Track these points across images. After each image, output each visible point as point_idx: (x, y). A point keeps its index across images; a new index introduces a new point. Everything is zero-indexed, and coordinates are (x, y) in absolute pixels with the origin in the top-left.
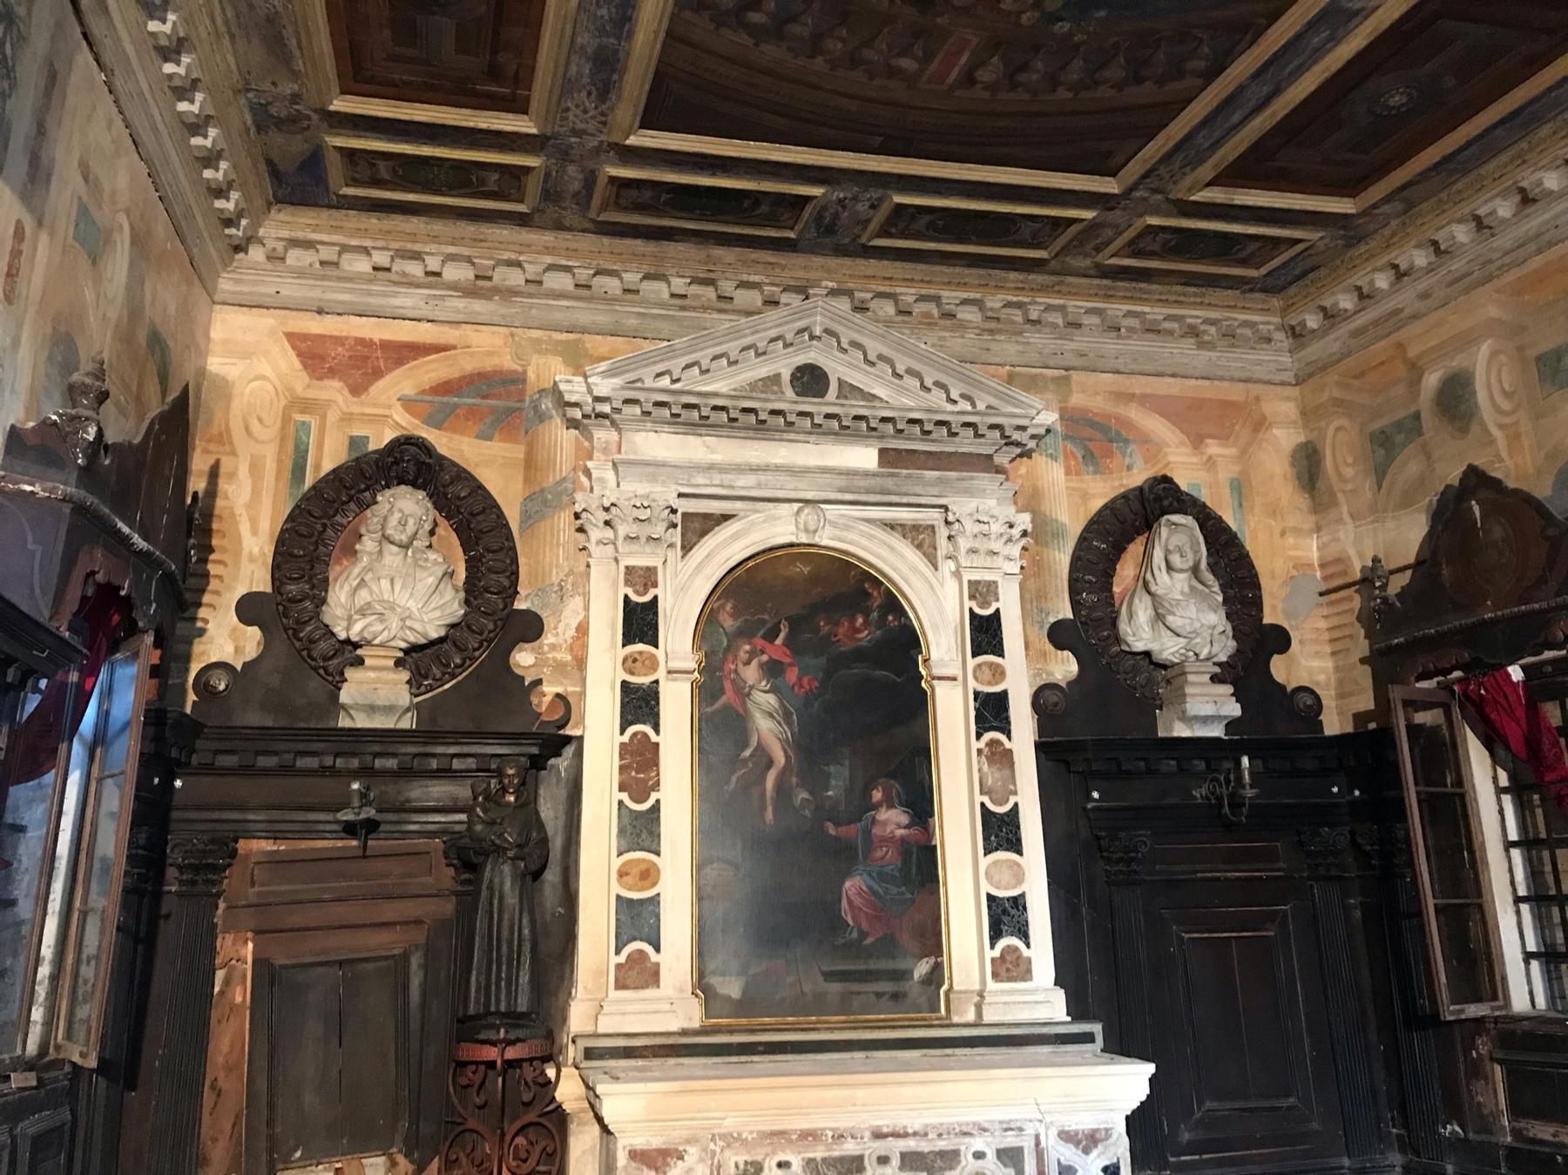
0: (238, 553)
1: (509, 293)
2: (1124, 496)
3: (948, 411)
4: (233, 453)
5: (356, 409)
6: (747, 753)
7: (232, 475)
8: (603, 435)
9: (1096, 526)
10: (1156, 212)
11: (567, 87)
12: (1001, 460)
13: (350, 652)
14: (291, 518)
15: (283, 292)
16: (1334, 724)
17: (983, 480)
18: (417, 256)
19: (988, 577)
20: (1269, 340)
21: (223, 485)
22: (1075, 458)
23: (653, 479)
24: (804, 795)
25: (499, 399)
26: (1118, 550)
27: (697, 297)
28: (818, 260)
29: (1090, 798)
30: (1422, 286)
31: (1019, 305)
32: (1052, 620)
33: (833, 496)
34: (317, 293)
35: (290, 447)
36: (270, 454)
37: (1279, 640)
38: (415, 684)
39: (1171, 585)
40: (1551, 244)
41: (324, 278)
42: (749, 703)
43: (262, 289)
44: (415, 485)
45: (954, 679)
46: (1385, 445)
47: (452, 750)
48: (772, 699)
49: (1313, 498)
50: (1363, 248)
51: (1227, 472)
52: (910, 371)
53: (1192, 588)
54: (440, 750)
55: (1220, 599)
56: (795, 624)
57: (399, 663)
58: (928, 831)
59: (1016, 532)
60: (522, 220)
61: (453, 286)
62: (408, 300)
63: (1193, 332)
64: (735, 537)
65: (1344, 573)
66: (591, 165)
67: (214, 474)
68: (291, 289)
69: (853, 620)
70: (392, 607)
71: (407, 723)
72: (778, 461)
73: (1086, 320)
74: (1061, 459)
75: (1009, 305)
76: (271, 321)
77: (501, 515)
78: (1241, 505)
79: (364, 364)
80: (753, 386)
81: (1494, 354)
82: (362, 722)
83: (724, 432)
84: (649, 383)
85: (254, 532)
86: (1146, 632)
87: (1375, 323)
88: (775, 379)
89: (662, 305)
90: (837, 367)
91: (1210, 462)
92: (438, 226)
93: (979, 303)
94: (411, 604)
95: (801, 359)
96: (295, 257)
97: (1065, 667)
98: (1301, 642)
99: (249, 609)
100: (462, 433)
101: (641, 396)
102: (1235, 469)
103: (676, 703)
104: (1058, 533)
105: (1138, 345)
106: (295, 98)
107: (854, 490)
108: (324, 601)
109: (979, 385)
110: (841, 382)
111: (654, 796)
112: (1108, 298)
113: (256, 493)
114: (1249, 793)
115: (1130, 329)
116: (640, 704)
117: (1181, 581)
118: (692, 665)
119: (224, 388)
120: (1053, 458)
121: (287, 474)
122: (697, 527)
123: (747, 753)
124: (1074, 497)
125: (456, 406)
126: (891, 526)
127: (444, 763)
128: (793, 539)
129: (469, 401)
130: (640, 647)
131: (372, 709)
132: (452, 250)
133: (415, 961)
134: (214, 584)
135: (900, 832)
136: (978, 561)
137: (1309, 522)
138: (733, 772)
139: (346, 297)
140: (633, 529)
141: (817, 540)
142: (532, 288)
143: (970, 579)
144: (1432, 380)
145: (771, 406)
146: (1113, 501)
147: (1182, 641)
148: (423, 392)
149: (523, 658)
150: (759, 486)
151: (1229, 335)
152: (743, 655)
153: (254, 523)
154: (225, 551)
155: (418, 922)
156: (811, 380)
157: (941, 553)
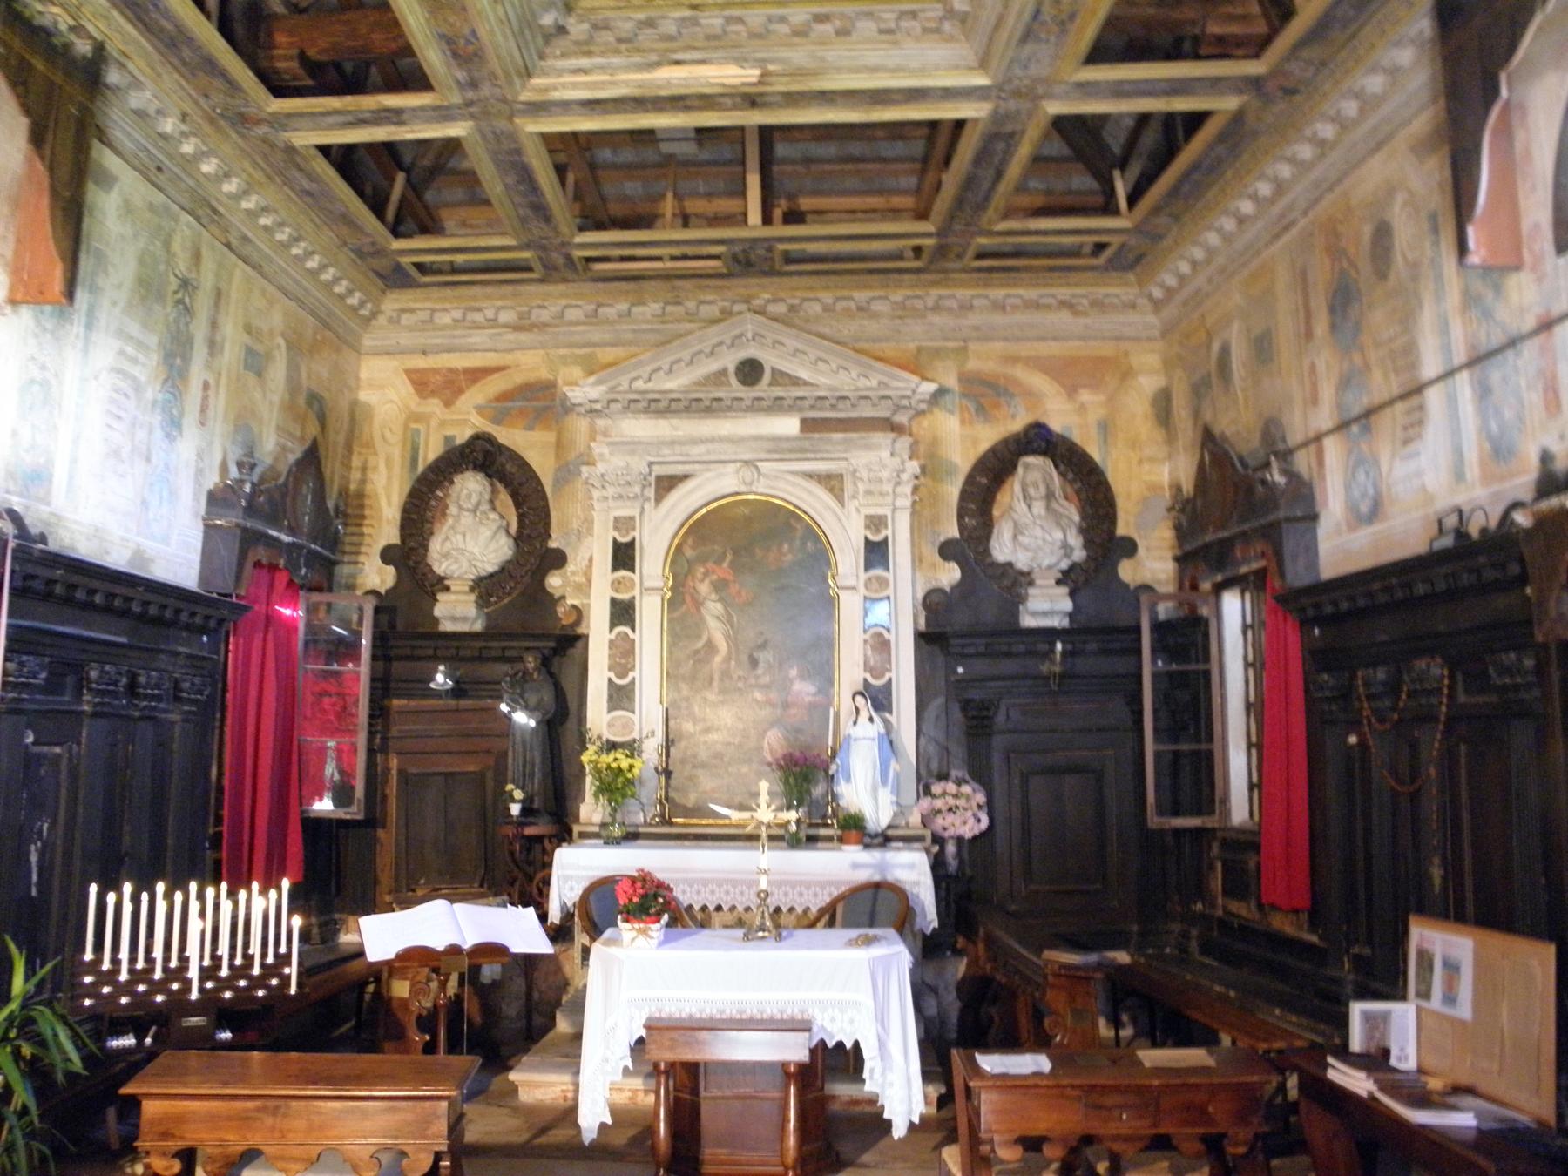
1: (542, 326)
4: (376, 454)
5: (448, 417)
7: (375, 468)
13: (441, 584)
17: (882, 439)
19: (880, 511)
21: (371, 475)
25: (538, 399)
29: (955, 672)
32: (942, 539)
34: (422, 341)
35: (409, 447)
37: (1129, 548)
42: (703, 611)
45: (854, 588)
46: (1199, 390)
48: (719, 606)
51: (1094, 416)
57: (472, 589)
61: (506, 326)
62: (478, 338)
63: (1064, 304)
64: (693, 491)
67: (364, 469)
68: (405, 339)
69: (780, 545)
70: (463, 551)
71: (478, 627)
78: (1105, 441)
79: (449, 386)
89: (648, 322)
90: (770, 359)
91: (1082, 409)
92: (489, 290)
94: (476, 550)
96: (406, 319)
97: (949, 575)
98: (1148, 549)
99: (388, 555)
101: (619, 397)
103: (650, 612)
104: (951, 470)
105: (1021, 317)
110: (773, 370)
113: (389, 478)
116: (623, 613)
119: (368, 411)
120: (951, 412)
121: (407, 464)
122: (667, 484)
124: (963, 441)
126: (810, 476)
127: (499, 653)
128: (736, 489)
130: (623, 573)
131: (454, 619)
132: (499, 303)
134: (367, 540)
135: (808, 699)
136: (871, 500)
139: (438, 341)
144: (1216, 347)
147: (1030, 554)
149: (554, 581)
150: (709, 452)
152: (699, 576)
155: (488, 752)
156: (750, 371)
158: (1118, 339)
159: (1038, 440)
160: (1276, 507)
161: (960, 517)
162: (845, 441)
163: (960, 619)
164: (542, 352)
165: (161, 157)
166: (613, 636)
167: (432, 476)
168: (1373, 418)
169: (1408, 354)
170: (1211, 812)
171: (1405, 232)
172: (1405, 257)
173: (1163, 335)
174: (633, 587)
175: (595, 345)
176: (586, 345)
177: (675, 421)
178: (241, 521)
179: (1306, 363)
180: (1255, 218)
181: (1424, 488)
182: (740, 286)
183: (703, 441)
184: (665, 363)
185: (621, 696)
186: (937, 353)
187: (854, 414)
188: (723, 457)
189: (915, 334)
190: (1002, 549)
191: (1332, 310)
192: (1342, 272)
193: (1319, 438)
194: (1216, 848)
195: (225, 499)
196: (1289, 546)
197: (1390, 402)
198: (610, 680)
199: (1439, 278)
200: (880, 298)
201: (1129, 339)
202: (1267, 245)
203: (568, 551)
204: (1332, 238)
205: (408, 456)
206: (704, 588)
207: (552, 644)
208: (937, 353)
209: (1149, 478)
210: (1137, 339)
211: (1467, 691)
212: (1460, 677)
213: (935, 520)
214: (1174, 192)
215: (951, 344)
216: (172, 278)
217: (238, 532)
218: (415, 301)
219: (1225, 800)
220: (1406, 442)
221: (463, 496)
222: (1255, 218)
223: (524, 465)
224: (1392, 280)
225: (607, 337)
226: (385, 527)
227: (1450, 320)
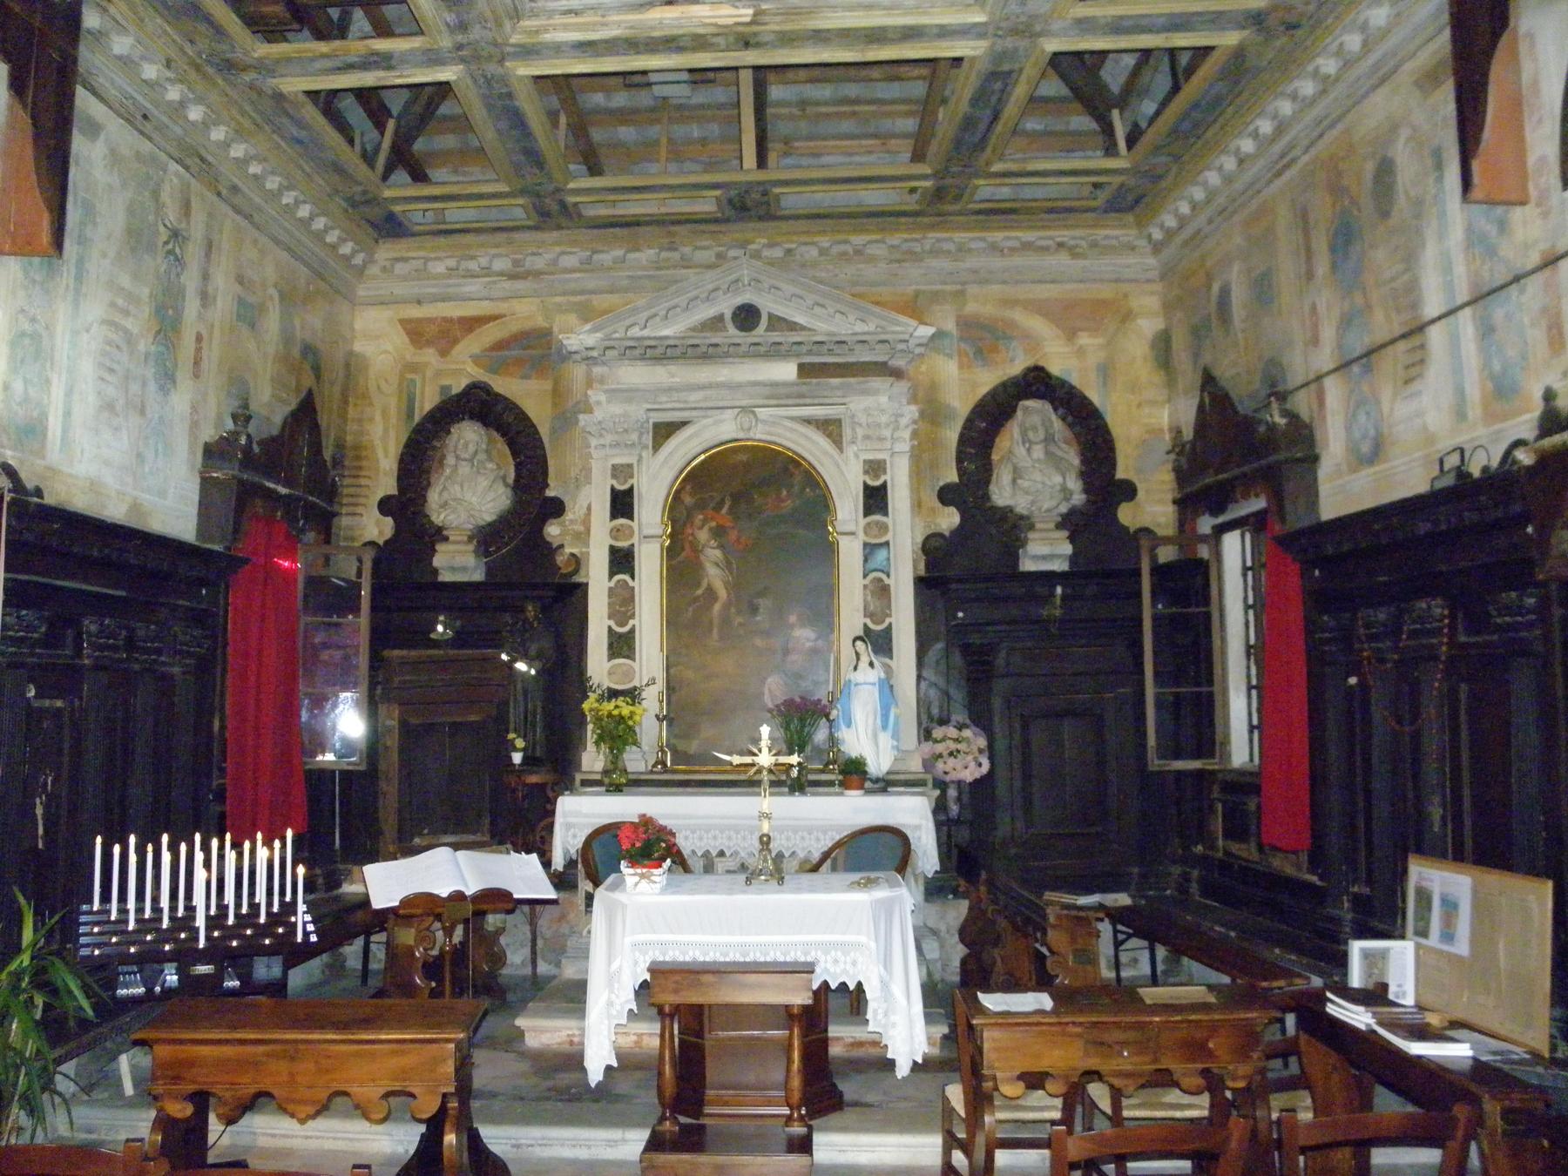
0: (377, 470)
1: (537, 274)
2: (1004, 385)
4: (371, 404)
6: (699, 592)
7: (371, 420)
13: (439, 534)
14: (407, 446)
16: (433, 636)
17: (877, 383)
18: (473, 258)
22: (967, 354)
23: (629, 401)
29: (955, 617)
33: (761, 402)
34: (416, 290)
35: (405, 397)
36: (393, 402)
37: (1128, 491)
45: (853, 534)
46: (1198, 333)
48: (718, 553)
51: (1094, 358)
55: (1076, 461)
56: (736, 498)
59: (904, 421)
61: (501, 274)
62: (473, 287)
64: (690, 438)
72: (721, 379)
74: (956, 358)
75: (906, 240)
86: (1008, 489)
88: (720, 318)
89: (644, 268)
90: (768, 304)
91: (1081, 352)
92: (483, 238)
94: (474, 499)
95: (740, 300)
96: (400, 268)
97: (949, 519)
99: (385, 506)
100: (511, 375)
104: (950, 414)
110: (771, 316)
111: (631, 622)
113: (386, 430)
115: (1012, 250)
116: (622, 560)
120: (950, 356)
122: (664, 432)
123: (699, 592)
124: (963, 385)
126: (808, 421)
128: (734, 436)
130: (622, 521)
131: (453, 569)
141: (752, 435)
143: (876, 458)
144: (1216, 288)
145: (708, 342)
149: (553, 530)
150: (706, 399)
156: (747, 316)
159: (1037, 383)
161: (959, 461)
164: (537, 300)
165: (149, 106)
166: (612, 584)
168: (1374, 357)
170: (1212, 755)
173: (1163, 277)
174: (631, 535)
176: (582, 293)
177: (673, 368)
178: (236, 472)
181: (1425, 428)
185: (622, 645)
186: (936, 297)
188: (721, 404)
189: (914, 278)
190: (1002, 494)
191: (1333, 249)
197: (1393, 341)
199: (1442, 214)
203: (566, 500)
205: (404, 406)
206: (703, 536)
207: (551, 593)
208: (936, 297)
209: (1149, 422)
212: (1460, 615)
213: (934, 465)
215: (948, 288)
216: (162, 229)
218: (409, 250)
219: (1226, 741)
220: (1407, 382)
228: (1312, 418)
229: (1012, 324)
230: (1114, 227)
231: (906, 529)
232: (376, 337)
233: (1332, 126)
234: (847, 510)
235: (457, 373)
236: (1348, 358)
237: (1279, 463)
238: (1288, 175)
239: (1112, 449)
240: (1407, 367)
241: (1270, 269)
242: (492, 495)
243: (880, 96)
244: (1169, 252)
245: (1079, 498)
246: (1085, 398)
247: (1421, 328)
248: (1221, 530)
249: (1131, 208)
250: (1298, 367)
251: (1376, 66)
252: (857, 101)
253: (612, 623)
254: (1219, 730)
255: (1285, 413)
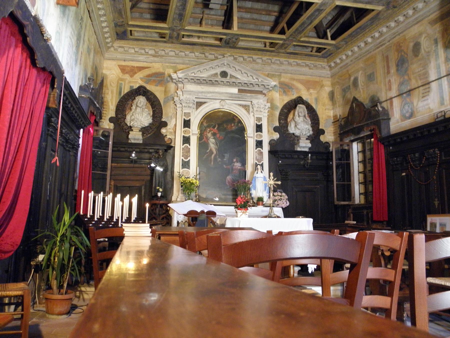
0: (109, 109)
2: (291, 101)
3: (253, 81)
4: (108, 89)
5: (131, 80)
7: (108, 94)
8: (180, 85)
9: (285, 107)
10: (295, 41)
11: (174, 19)
12: (265, 92)
13: (130, 128)
14: (119, 102)
15: (118, 57)
17: (260, 96)
19: (260, 116)
20: (325, 68)
23: (190, 94)
24: (219, 160)
25: (160, 78)
26: (289, 112)
27: (201, 56)
28: (226, 49)
29: (279, 162)
30: (351, 59)
31: (270, 59)
33: (228, 98)
34: (124, 57)
35: (119, 88)
37: (323, 132)
38: (143, 135)
39: (299, 120)
40: (370, 52)
41: (125, 54)
43: (113, 56)
44: (143, 96)
46: (345, 91)
47: (150, 147)
48: (214, 140)
49: (333, 102)
50: (340, 50)
52: (245, 73)
53: (304, 120)
54: (147, 147)
55: (310, 123)
56: (219, 125)
57: (140, 131)
58: (245, 168)
59: (267, 107)
60: (165, 42)
61: (151, 55)
62: (142, 58)
65: (337, 118)
66: (178, 32)
68: (119, 56)
69: (231, 124)
71: (141, 142)
72: (216, 91)
73: (284, 63)
74: (278, 92)
75: (268, 59)
76: (115, 63)
77: (159, 101)
79: (133, 71)
80: (212, 75)
81: (362, 74)
82: (133, 141)
83: (205, 85)
84: (190, 75)
85: (112, 105)
87: (344, 66)
88: (217, 74)
89: (193, 58)
90: (230, 71)
91: (311, 94)
92: (148, 43)
93: (261, 59)
97: (276, 136)
98: (327, 133)
99: (111, 120)
101: (188, 77)
102: (316, 96)
103: (194, 141)
104: (277, 108)
106: (123, 22)
107: (232, 97)
108: (125, 118)
109: (259, 76)
110: (231, 75)
111: (189, 158)
112: (289, 58)
113: (112, 97)
114: (309, 161)
115: (294, 65)
116: (186, 140)
117: (301, 119)
118: (197, 133)
119: (106, 75)
120: (277, 92)
122: (199, 104)
123: (208, 151)
124: (281, 100)
125: (151, 79)
126: (240, 105)
128: (219, 107)
129: (153, 78)
130: (187, 129)
131: (135, 139)
132: (151, 48)
133: (143, 187)
135: (239, 168)
136: (258, 113)
137: (331, 107)
138: (205, 154)
140: (185, 105)
141: (224, 107)
142: (167, 55)
143: (257, 117)
144: (352, 78)
146: (289, 101)
148: (145, 77)
149: (163, 131)
150: (212, 96)
151: (315, 66)
152: (208, 131)
153: (112, 103)
154: (106, 108)
155: (143, 180)
156: (224, 74)
157: (250, 111)
158: (320, 77)
159: (299, 101)
160: (379, 116)
162: (251, 96)
163: (279, 148)
164: (161, 64)
167: (126, 97)
168: (411, 92)
169: (426, 74)
170: (350, 201)
171: (425, 44)
172: (425, 50)
173: (332, 77)
174: (190, 133)
175: (177, 63)
176: (174, 63)
177: (202, 87)
178: (89, 96)
179: (387, 80)
180: (371, 43)
181: (429, 108)
182: (222, 51)
183: (211, 93)
184: (201, 69)
185: (186, 165)
187: (253, 89)
190: (292, 129)
191: (397, 66)
192: (402, 55)
193: (391, 99)
194: (350, 211)
195: (85, 89)
196: (383, 126)
197: (418, 87)
198: (182, 159)
200: (260, 58)
201: (323, 77)
202: (374, 50)
204: (399, 47)
205: (118, 90)
206: (209, 135)
209: (328, 113)
210: (325, 77)
211: (444, 157)
212: (443, 153)
213: (272, 121)
214: (350, 36)
215: (277, 73)
217: (88, 99)
218: (125, 44)
219: (354, 197)
221: (139, 103)
222: (371, 43)
223: (155, 96)
224: (420, 56)
225: (181, 61)
226: (110, 110)
227: (441, 66)
228: (388, 109)
229: (293, 85)
230: (321, 62)
231: (267, 137)
232: (111, 71)
233: (399, 34)
234: (250, 131)
235: (136, 82)
236: (402, 92)
237: (380, 120)
238: (381, 48)
239: (319, 120)
240: (423, 93)
241: (373, 73)
242: (147, 119)
243: (262, 19)
244: (333, 71)
245: (311, 133)
246: (312, 106)
247: (429, 83)
248: (352, 141)
249: (326, 57)
250: (383, 96)
251: (416, 19)
252: (256, 20)
253: (183, 158)
254: (352, 193)
255: (382, 107)
